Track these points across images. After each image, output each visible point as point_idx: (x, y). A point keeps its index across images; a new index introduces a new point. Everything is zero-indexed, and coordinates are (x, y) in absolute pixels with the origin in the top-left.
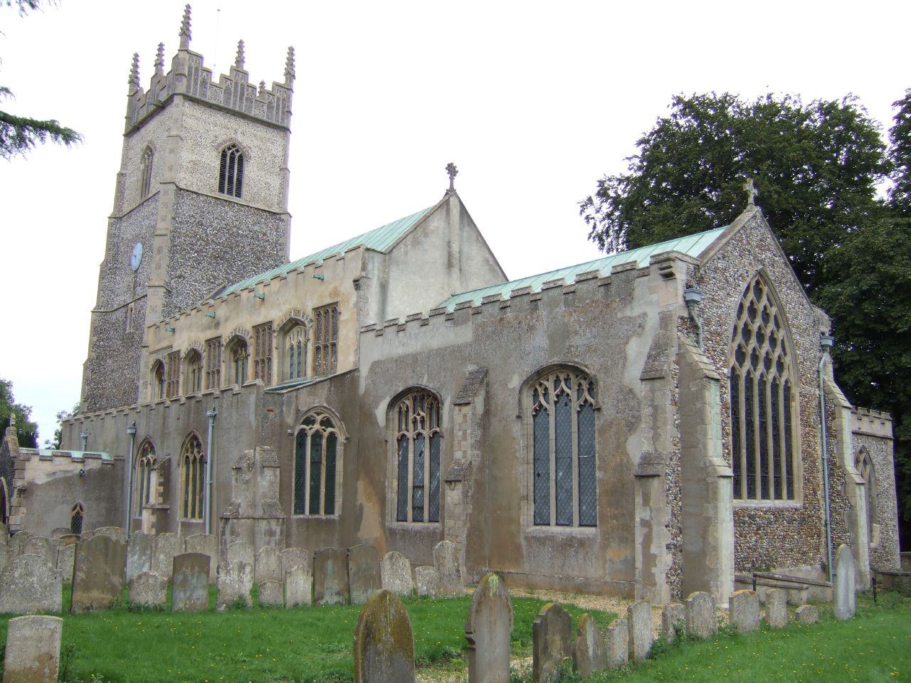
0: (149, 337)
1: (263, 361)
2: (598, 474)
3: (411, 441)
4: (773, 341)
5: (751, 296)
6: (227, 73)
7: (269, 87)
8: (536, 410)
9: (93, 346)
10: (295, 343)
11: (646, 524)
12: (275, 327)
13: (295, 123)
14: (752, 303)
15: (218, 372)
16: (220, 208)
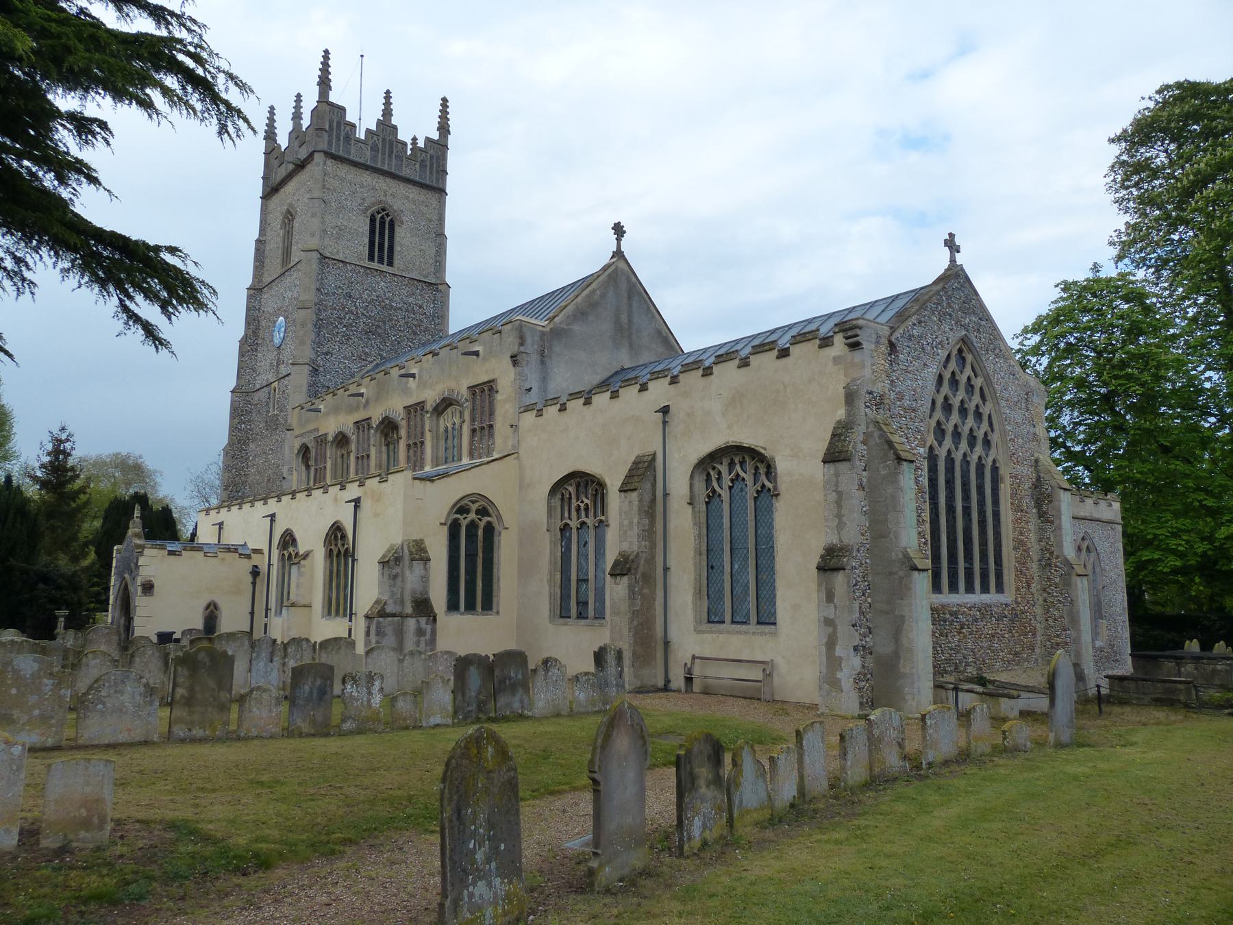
0: (293, 419)
4: (978, 415)
5: (953, 365)
7: (421, 144)
8: (708, 496)
10: (449, 425)
12: (429, 407)
13: (451, 184)
15: (368, 456)
16: (370, 279)
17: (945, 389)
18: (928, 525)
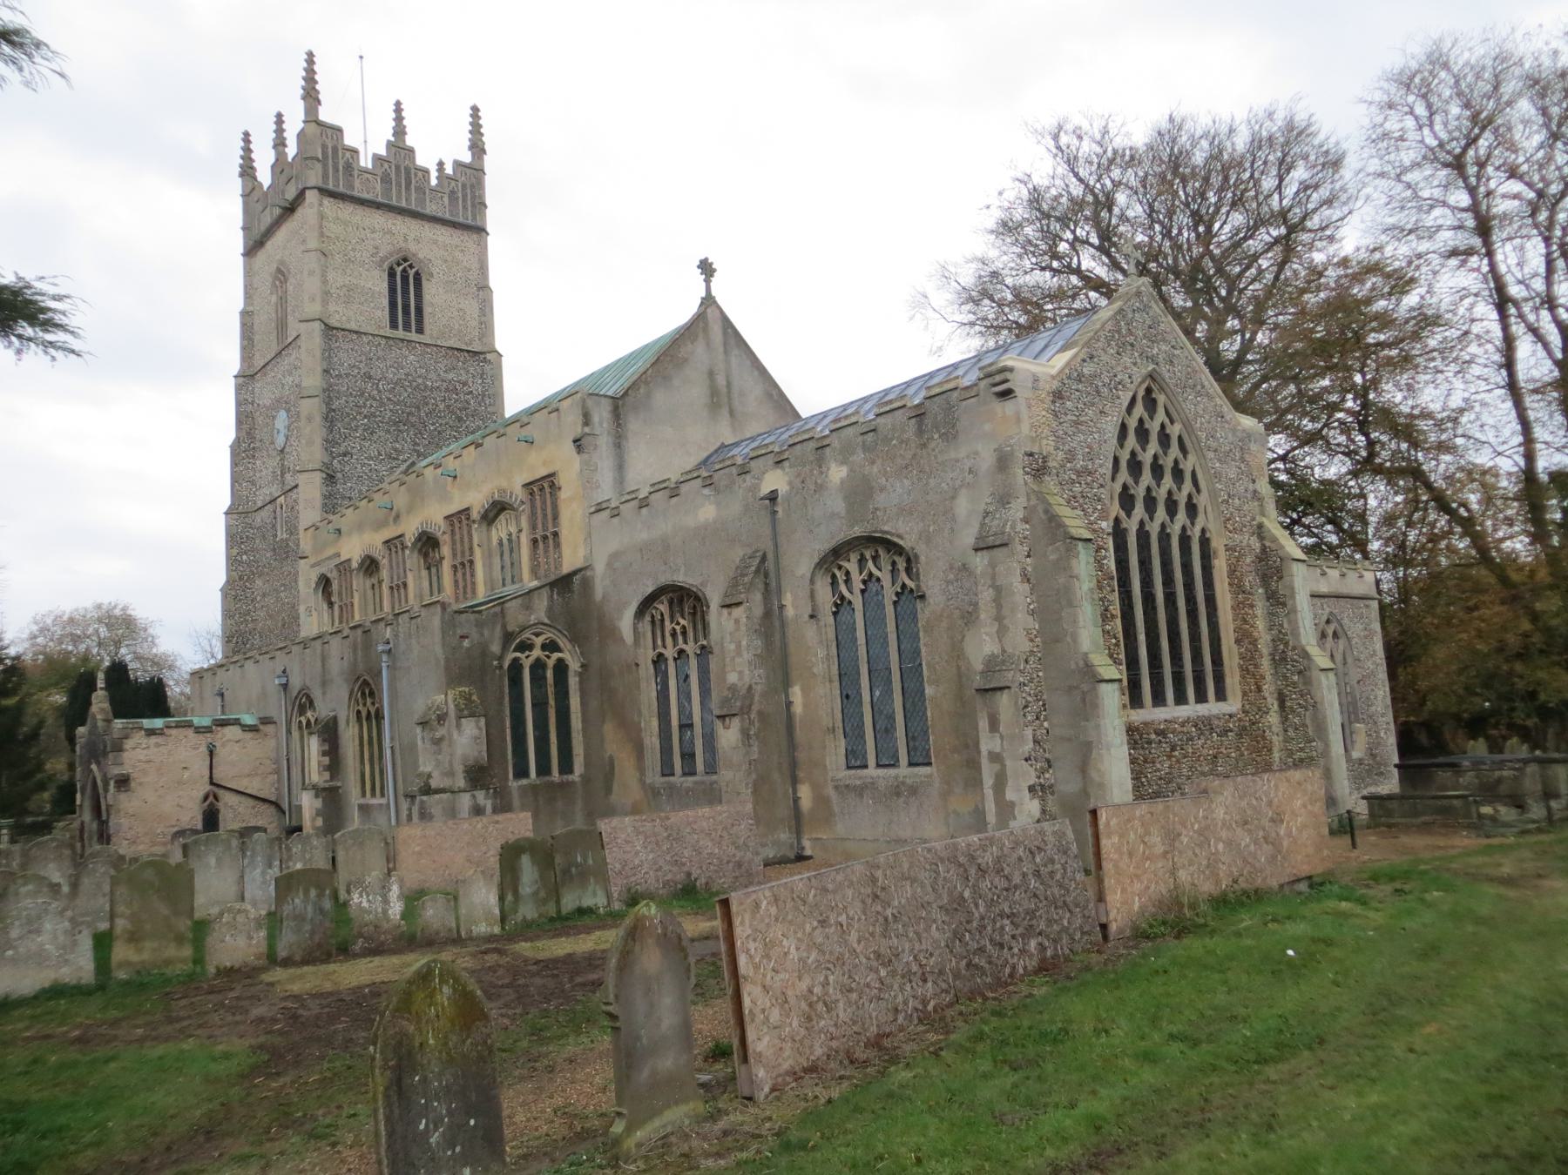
0: (306, 543)
1: (463, 564)
2: (929, 691)
3: (671, 663)
4: (1178, 474)
5: (1139, 410)
6: (383, 152)
7: (449, 170)
8: (836, 605)
9: (233, 562)
10: (504, 536)
11: (995, 757)
12: (475, 515)
13: (492, 220)
14: (1141, 421)
15: (405, 585)
17: (1131, 441)
18: (1118, 621)
